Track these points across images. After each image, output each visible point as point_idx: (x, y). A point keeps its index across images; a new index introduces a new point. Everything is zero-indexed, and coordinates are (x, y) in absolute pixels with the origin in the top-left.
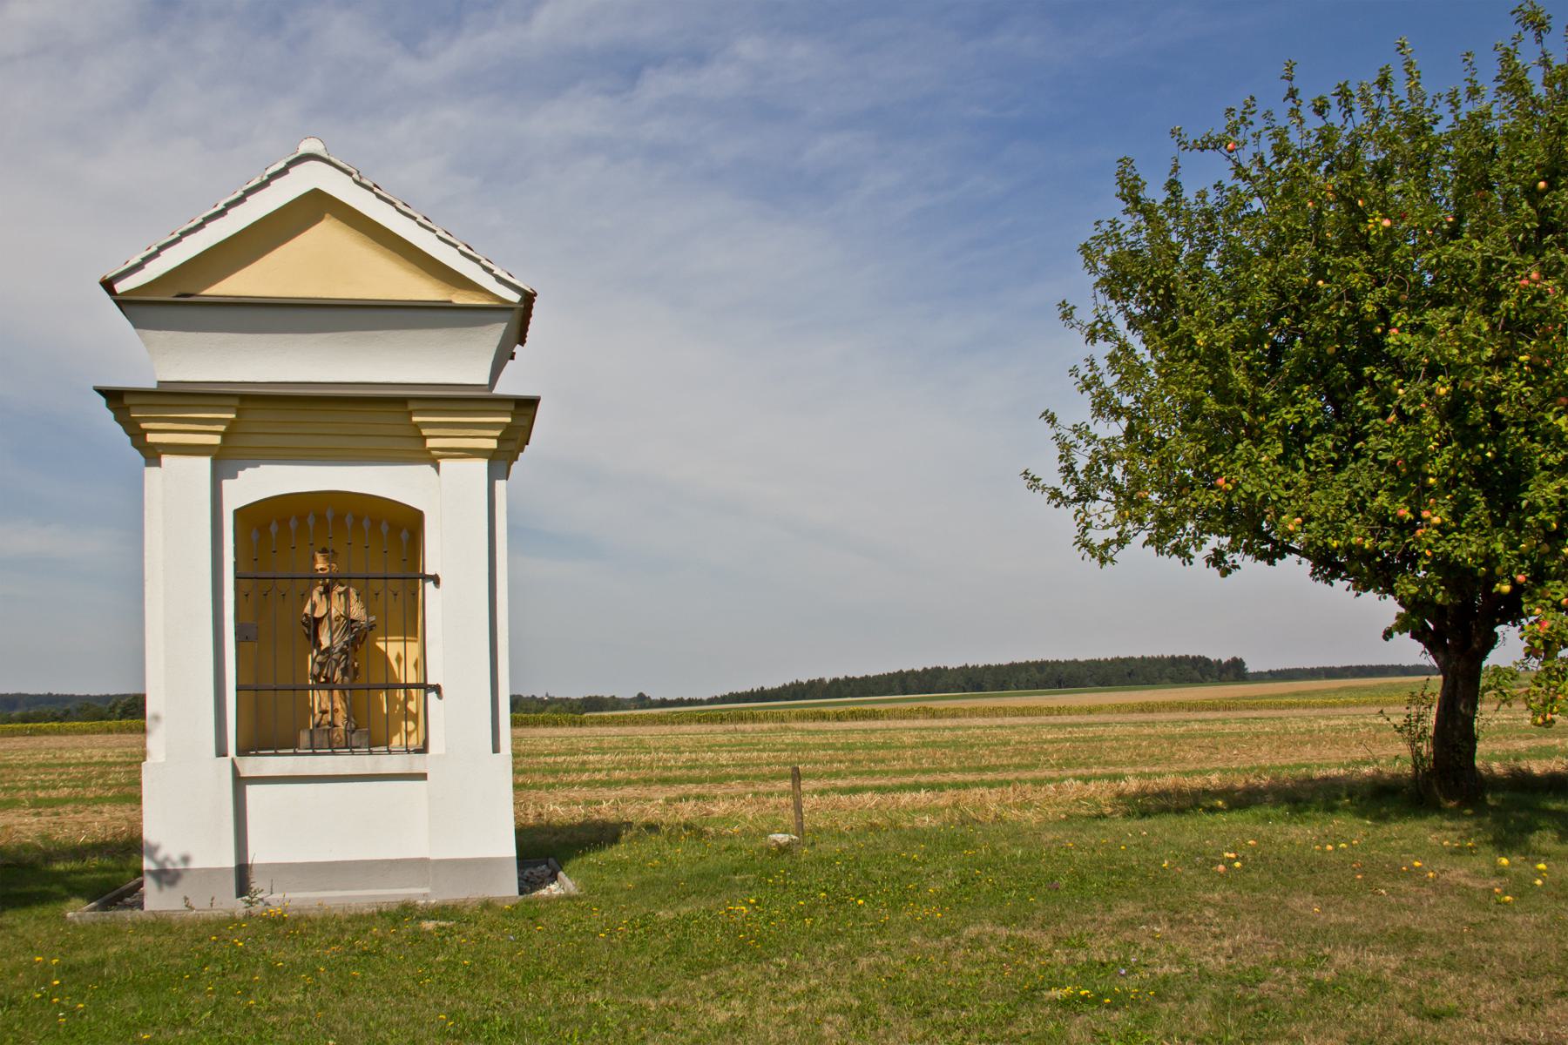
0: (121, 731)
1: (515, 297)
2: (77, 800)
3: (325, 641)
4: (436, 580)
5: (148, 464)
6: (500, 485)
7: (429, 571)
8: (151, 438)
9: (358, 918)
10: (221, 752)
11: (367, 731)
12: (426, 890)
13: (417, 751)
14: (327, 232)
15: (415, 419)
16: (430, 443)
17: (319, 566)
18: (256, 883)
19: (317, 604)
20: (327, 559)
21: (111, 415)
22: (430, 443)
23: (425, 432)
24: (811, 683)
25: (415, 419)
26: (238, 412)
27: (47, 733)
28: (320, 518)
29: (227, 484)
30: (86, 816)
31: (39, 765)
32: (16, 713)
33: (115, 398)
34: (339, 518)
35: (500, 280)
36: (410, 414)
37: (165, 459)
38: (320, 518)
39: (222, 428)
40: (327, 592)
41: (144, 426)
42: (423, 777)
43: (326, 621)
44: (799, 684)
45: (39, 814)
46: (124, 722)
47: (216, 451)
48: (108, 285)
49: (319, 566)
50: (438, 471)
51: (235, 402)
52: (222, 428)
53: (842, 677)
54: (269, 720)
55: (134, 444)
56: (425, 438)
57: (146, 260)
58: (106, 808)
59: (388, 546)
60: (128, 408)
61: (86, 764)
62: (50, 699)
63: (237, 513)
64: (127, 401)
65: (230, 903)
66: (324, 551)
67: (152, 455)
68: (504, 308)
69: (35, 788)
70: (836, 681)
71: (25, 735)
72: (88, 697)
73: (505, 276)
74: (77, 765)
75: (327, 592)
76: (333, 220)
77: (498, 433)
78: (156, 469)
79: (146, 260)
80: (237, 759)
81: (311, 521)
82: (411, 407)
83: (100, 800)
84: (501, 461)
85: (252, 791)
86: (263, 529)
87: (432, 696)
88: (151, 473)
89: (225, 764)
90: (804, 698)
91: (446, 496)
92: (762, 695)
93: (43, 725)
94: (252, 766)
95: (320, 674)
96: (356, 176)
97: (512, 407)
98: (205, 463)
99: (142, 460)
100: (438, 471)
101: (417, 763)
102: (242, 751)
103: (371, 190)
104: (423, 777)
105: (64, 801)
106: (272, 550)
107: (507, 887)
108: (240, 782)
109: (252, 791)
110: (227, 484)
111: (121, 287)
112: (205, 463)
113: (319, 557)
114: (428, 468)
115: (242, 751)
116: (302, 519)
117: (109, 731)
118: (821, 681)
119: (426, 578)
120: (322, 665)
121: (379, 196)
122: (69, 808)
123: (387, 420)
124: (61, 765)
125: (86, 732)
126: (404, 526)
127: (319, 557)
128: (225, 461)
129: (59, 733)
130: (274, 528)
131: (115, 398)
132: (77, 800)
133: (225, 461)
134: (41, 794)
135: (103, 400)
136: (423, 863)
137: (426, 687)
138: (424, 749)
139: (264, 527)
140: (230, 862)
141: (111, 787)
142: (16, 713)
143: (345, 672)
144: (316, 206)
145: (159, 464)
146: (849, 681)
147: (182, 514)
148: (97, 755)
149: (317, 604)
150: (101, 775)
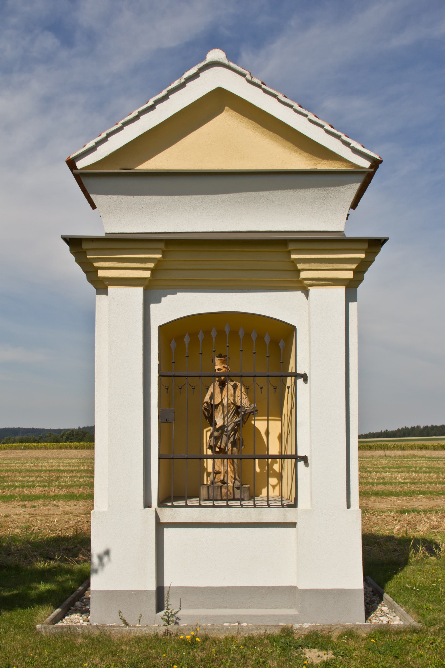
0: (66, 448)
1: (366, 164)
2: (46, 497)
3: (219, 422)
4: (305, 377)
5: (98, 293)
6: (353, 306)
7: (300, 371)
8: (101, 274)
9: (250, 641)
10: (147, 505)
11: (246, 490)
12: (292, 612)
13: (289, 506)
14: (226, 122)
15: (293, 256)
16: (303, 275)
17: (217, 367)
18: (172, 603)
19: (214, 394)
20: (223, 362)
21: (72, 258)
22: (303, 275)
23: (300, 266)
24: (413, 428)
25: (293, 256)
26: (163, 253)
27: (32, 448)
28: (194, 335)
29: (153, 307)
30: (50, 509)
31: (27, 471)
32: (18, 437)
33: (75, 244)
34: (234, 333)
35: (355, 151)
36: (289, 253)
37: (111, 289)
38: (234, 333)
39: (151, 265)
40: (222, 385)
41: (96, 264)
42: (294, 525)
43: (220, 407)
44: (406, 429)
45: (24, 506)
46: (68, 443)
47: (147, 283)
48: (71, 163)
49: (217, 367)
50: (307, 296)
51: (162, 246)
52: (151, 265)
53: (429, 425)
54: (177, 481)
55: (89, 279)
56: (299, 271)
57: (98, 144)
58: (61, 503)
59: (268, 351)
60: (85, 253)
61: (50, 471)
62: (33, 431)
63: (161, 328)
64: (85, 246)
65: (152, 623)
66: (220, 356)
67: (101, 285)
68: (354, 172)
69: (23, 487)
70: (426, 427)
71: (21, 449)
72: (50, 430)
73: (359, 147)
74: (45, 471)
75: (222, 385)
76: (231, 111)
77: (354, 266)
78: (104, 296)
79: (98, 144)
80: (159, 510)
81: (214, 334)
82: (291, 247)
83: (57, 497)
84: (351, 288)
85: (167, 532)
86: (179, 339)
87: (301, 464)
88: (101, 299)
89: (151, 512)
90: (409, 436)
91: (315, 317)
92: (386, 434)
93: (30, 444)
94: (169, 514)
95: (215, 446)
96: (248, 77)
97: (365, 246)
98: (139, 291)
99: (94, 290)
100: (307, 296)
101: (288, 515)
102: (162, 503)
103: (259, 87)
104: (294, 525)
105: (37, 497)
106: (184, 353)
107: (355, 616)
108: (160, 526)
109: (167, 532)
110: (153, 307)
111: (80, 164)
112: (139, 291)
113: (217, 360)
114: (299, 294)
115: (162, 503)
116: (194, 335)
117: (61, 448)
118: (418, 427)
119: (297, 376)
120: (217, 439)
121: (265, 91)
122: (41, 502)
123: (272, 258)
124: (37, 471)
125: (50, 448)
126: (279, 338)
127: (217, 360)
128: (153, 291)
129: (37, 448)
130: (187, 340)
131: (75, 244)
132: (46, 497)
133: (153, 291)
134: (26, 492)
135: (67, 247)
136: (291, 590)
137: (297, 458)
138: (295, 505)
139: (180, 339)
140: (152, 587)
141: (63, 487)
142: (18, 437)
143: (234, 444)
144: (219, 100)
145: (106, 294)
146: (433, 427)
147: (122, 329)
148: (55, 464)
149: (214, 394)
150: (58, 478)
